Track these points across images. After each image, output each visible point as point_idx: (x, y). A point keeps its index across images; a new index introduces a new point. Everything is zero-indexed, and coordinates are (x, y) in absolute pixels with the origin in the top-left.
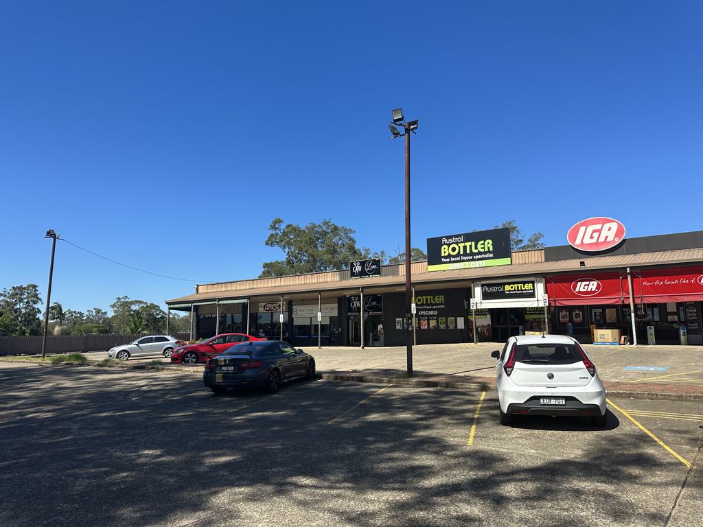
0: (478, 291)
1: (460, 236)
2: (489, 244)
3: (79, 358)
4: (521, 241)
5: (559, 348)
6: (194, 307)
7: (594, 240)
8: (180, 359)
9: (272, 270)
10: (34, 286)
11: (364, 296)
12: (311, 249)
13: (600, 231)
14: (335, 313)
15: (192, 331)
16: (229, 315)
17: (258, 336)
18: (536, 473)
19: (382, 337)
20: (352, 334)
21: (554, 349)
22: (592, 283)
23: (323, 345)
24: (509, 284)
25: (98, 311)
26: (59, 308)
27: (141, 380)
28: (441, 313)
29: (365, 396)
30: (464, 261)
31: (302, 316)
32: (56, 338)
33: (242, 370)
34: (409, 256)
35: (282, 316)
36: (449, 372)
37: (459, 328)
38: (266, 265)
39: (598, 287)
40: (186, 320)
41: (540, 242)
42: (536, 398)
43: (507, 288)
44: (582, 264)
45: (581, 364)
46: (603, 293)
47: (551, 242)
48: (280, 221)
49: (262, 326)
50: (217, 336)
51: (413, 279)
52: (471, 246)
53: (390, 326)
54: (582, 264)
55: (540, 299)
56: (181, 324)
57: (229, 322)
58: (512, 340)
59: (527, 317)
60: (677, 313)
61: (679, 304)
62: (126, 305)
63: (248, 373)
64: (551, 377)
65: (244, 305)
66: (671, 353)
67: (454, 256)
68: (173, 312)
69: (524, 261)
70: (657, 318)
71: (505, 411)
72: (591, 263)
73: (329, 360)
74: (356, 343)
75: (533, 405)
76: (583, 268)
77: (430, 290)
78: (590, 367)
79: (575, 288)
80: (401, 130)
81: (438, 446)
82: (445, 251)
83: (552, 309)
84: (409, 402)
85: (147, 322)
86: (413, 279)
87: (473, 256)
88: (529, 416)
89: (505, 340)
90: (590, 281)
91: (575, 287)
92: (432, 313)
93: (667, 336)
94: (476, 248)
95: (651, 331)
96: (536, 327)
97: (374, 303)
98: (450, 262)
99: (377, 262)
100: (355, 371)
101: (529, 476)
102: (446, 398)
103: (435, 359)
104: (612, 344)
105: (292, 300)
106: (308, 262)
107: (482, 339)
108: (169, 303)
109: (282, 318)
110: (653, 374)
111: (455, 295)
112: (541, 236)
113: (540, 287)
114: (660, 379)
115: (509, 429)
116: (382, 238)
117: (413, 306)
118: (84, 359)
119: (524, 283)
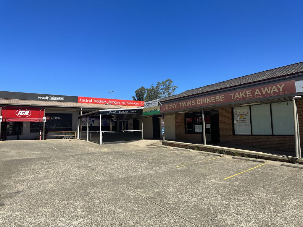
22: (27, 111)
39: (29, 114)
79: (17, 113)
87: (88, 103)
90: (26, 110)
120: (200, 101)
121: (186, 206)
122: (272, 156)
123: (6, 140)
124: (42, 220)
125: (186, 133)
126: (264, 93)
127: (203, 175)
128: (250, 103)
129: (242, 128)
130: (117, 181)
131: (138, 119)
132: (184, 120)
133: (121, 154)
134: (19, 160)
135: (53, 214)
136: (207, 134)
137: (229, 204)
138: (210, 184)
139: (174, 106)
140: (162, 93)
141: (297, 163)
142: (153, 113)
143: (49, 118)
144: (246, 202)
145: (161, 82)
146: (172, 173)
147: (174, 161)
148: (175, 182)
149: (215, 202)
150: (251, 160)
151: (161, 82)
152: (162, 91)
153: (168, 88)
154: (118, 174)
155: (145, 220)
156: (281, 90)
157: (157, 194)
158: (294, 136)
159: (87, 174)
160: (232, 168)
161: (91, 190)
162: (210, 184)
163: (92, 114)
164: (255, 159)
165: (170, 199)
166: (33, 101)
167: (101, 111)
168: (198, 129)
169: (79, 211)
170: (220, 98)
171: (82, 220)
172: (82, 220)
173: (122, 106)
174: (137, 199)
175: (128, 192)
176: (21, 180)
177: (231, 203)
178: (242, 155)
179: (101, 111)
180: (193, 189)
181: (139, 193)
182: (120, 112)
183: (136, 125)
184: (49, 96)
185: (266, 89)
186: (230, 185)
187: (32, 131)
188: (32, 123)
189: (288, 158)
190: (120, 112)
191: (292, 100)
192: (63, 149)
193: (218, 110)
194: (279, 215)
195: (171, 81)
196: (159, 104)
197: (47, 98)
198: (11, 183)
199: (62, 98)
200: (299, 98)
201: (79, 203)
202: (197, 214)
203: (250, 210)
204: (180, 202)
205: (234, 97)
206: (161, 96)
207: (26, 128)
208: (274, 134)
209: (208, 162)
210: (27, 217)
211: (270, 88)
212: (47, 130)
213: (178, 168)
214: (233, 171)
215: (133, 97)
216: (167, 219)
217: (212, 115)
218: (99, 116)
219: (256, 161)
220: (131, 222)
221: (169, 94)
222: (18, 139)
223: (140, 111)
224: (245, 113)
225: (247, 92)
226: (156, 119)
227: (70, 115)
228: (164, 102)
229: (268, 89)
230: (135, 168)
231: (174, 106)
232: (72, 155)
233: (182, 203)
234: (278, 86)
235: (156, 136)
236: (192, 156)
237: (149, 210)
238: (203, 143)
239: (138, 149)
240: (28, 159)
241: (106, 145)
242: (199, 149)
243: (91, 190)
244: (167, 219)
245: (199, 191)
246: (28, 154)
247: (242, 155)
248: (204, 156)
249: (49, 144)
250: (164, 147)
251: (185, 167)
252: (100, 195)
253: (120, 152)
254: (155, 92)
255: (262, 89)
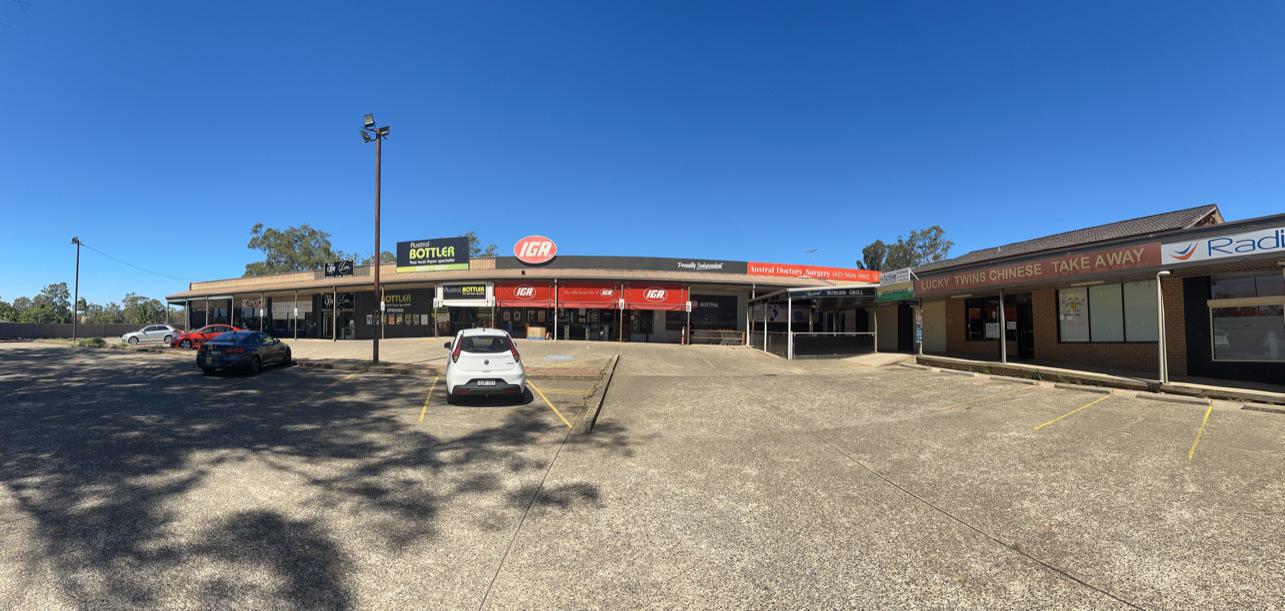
0: (440, 291)
1: (427, 241)
2: (451, 250)
3: (101, 341)
4: (480, 250)
5: (496, 339)
6: (187, 301)
7: (533, 255)
8: (177, 344)
9: (253, 270)
10: (65, 284)
11: (337, 295)
12: (288, 249)
13: (539, 247)
14: (310, 310)
15: (186, 321)
16: (216, 310)
17: (240, 327)
18: (465, 440)
19: (353, 332)
20: (325, 329)
21: (491, 341)
23: (298, 337)
24: (466, 286)
25: (114, 305)
26: (83, 302)
27: (141, 360)
28: (407, 311)
29: (332, 380)
30: (429, 264)
31: (280, 312)
32: (83, 326)
33: (228, 355)
34: (378, 259)
35: (262, 311)
36: (405, 362)
37: (422, 323)
38: (248, 266)
40: (181, 314)
41: (495, 252)
42: (474, 381)
43: (464, 289)
44: (523, 273)
45: (509, 353)
46: (536, 298)
47: (502, 253)
48: (261, 226)
49: (245, 320)
50: (207, 326)
51: (382, 279)
52: (436, 251)
53: (361, 322)
54: (523, 273)
55: (489, 300)
56: (177, 316)
57: (216, 315)
58: (460, 333)
59: (479, 315)
60: (585, 317)
61: (588, 310)
62: (134, 300)
63: (233, 358)
64: (487, 363)
65: (229, 301)
66: (577, 346)
67: (421, 260)
68: (171, 306)
69: (480, 267)
70: (572, 319)
71: (451, 392)
72: (531, 273)
73: (302, 349)
74: (329, 336)
75: (472, 387)
76: (524, 276)
77: (397, 290)
78: (517, 356)
80: (372, 135)
81: (393, 426)
82: (413, 254)
83: (498, 309)
84: (368, 385)
85: (150, 315)
86: (382, 279)
87: (436, 260)
88: (470, 396)
89: (455, 335)
91: (517, 291)
92: (399, 310)
93: (577, 334)
94: (440, 253)
95: (567, 329)
96: (485, 324)
97: (347, 301)
98: (418, 265)
99: (350, 263)
100: (326, 360)
101: (462, 445)
102: (398, 383)
103: (397, 351)
104: (541, 338)
105: (271, 298)
106: (286, 262)
107: (442, 334)
108: (168, 299)
109: (262, 313)
110: (562, 361)
111: (420, 295)
112: (496, 247)
113: (490, 290)
114: (567, 365)
115: (453, 407)
116: (358, 244)
117: (383, 303)
118: (104, 342)
119: (478, 286)
120: (996, 274)
121: (955, 487)
122: (1122, 381)
123: (629, 340)
124: (691, 491)
125: (967, 339)
126: (1111, 263)
127: (994, 424)
128: (1088, 281)
129: (1073, 329)
130: (820, 436)
131: (867, 310)
132: (964, 313)
133: (828, 381)
134: (651, 377)
135: (706, 486)
136: (1010, 342)
137: (1037, 478)
138: (1006, 440)
139: (943, 282)
140: (920, 256)
141: (1162, 391)
142: (899, 297)
143: (696, 304)
144: (1068, 471)
145: (919, 232)
146: (930, 423)
147: (939, 397)
148: (935, 440)
149: (1012, 475)
150: (1087, 390)
151: (919, 232)
152: (920, 251)
153: (934, 246)
154: (821, 422)
155: (871, 518)
156: (1139, 260)
157: (899, 463)
158: (1157, 343)
159: (764, 416)
160: (1052, 407)
161: (771, 449)
162: (1006, 440)
163: (773, 298)
164: (1094, 388)
165: (924, 475)
166: (507, 271)
167: (790, 290)
168: (991, 331)
169: (750, 487)
170: (1033, 269)
171: (755, 505)
172: (755, 505)
173: (833, 281)
174: (856, 475)
175: (840, 458)
176: (656, 414)
177: (1041, 476)
178: (1073, 380)
179: (790, 290)
180: (971, 452)
181: (861, 462)
182: (829, 293)
183: (863, 322)
184: (696, 261)
185: (1114, 255)
186: (1043, 440)
187: (668, 327)
188: (668, 313)
189: (1148, 383)
190: (829, 293)
191: (1156, 279)
192: (721, 364)
193: (1030, 294)
194: (1122, 489)
195: (942, 232)
196: (912, 277)
197: (693, 265)
198: (642, 416)
199: (720, 266)
200: (1166, 276)
201: (751, 471)
202: (975, 502)
203: (1074, 486)
204: (944, 480)
205: (1059, 268)
206: (917, 261)
207: (659, 323)
208: (1128, 340)
209: (1006, 397)
210: (668, 481)
211: (1121, 254)
212: (693, 326)
213: (946, 411)
214: (1053, 412)
215: (858, 263)
216: (914, 516)
217: (1020, 304)
218: (787, 303)
219: (1095, 391)
220: (844, 520)
221: (935, 258)
222: (647, 341)
223: (871, 291)
224: (1080, 300)
225: (1082, 259)
226: (905, 310)
227: (733, 300)
228: (921, 275)
229: (1118, 256)
230: (856, 410)
231: (943, 282)
232: (736, 377)
233: (947, 482)
234: (1135, 251)
235: (906, 345)
236: (978, 387)
237: (879, 498)
238: (1000, 360)
239: (865, 372)
240: (665, 377)
241: (799, 361)
242: (992, 371)
243: (771, 449)
244: (914, 516)
245: (983, 456)
246: (664, 369)
247: (1073, 380)
248: (1001, 384)
249: (699, 352)
250: (920, 369)
251: (962, 409)
252: (788, 459)
253: (828, 377)
254: (905, 252)
255: (1108, 255)
